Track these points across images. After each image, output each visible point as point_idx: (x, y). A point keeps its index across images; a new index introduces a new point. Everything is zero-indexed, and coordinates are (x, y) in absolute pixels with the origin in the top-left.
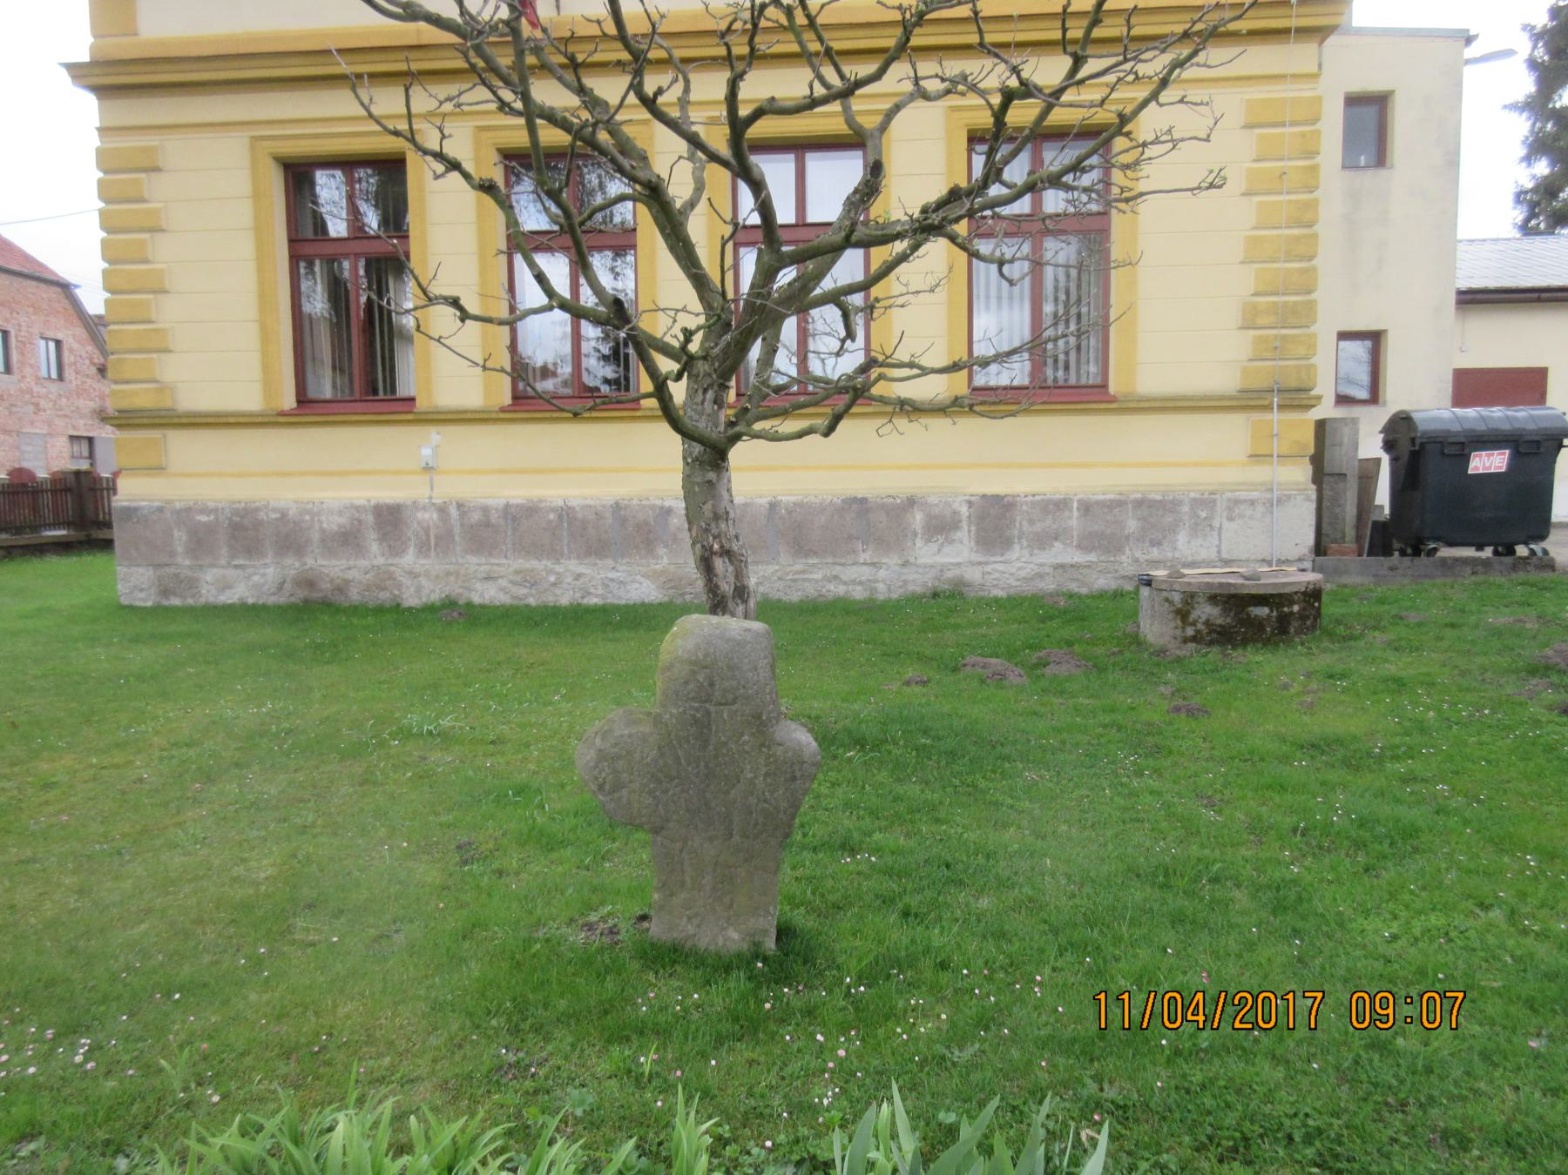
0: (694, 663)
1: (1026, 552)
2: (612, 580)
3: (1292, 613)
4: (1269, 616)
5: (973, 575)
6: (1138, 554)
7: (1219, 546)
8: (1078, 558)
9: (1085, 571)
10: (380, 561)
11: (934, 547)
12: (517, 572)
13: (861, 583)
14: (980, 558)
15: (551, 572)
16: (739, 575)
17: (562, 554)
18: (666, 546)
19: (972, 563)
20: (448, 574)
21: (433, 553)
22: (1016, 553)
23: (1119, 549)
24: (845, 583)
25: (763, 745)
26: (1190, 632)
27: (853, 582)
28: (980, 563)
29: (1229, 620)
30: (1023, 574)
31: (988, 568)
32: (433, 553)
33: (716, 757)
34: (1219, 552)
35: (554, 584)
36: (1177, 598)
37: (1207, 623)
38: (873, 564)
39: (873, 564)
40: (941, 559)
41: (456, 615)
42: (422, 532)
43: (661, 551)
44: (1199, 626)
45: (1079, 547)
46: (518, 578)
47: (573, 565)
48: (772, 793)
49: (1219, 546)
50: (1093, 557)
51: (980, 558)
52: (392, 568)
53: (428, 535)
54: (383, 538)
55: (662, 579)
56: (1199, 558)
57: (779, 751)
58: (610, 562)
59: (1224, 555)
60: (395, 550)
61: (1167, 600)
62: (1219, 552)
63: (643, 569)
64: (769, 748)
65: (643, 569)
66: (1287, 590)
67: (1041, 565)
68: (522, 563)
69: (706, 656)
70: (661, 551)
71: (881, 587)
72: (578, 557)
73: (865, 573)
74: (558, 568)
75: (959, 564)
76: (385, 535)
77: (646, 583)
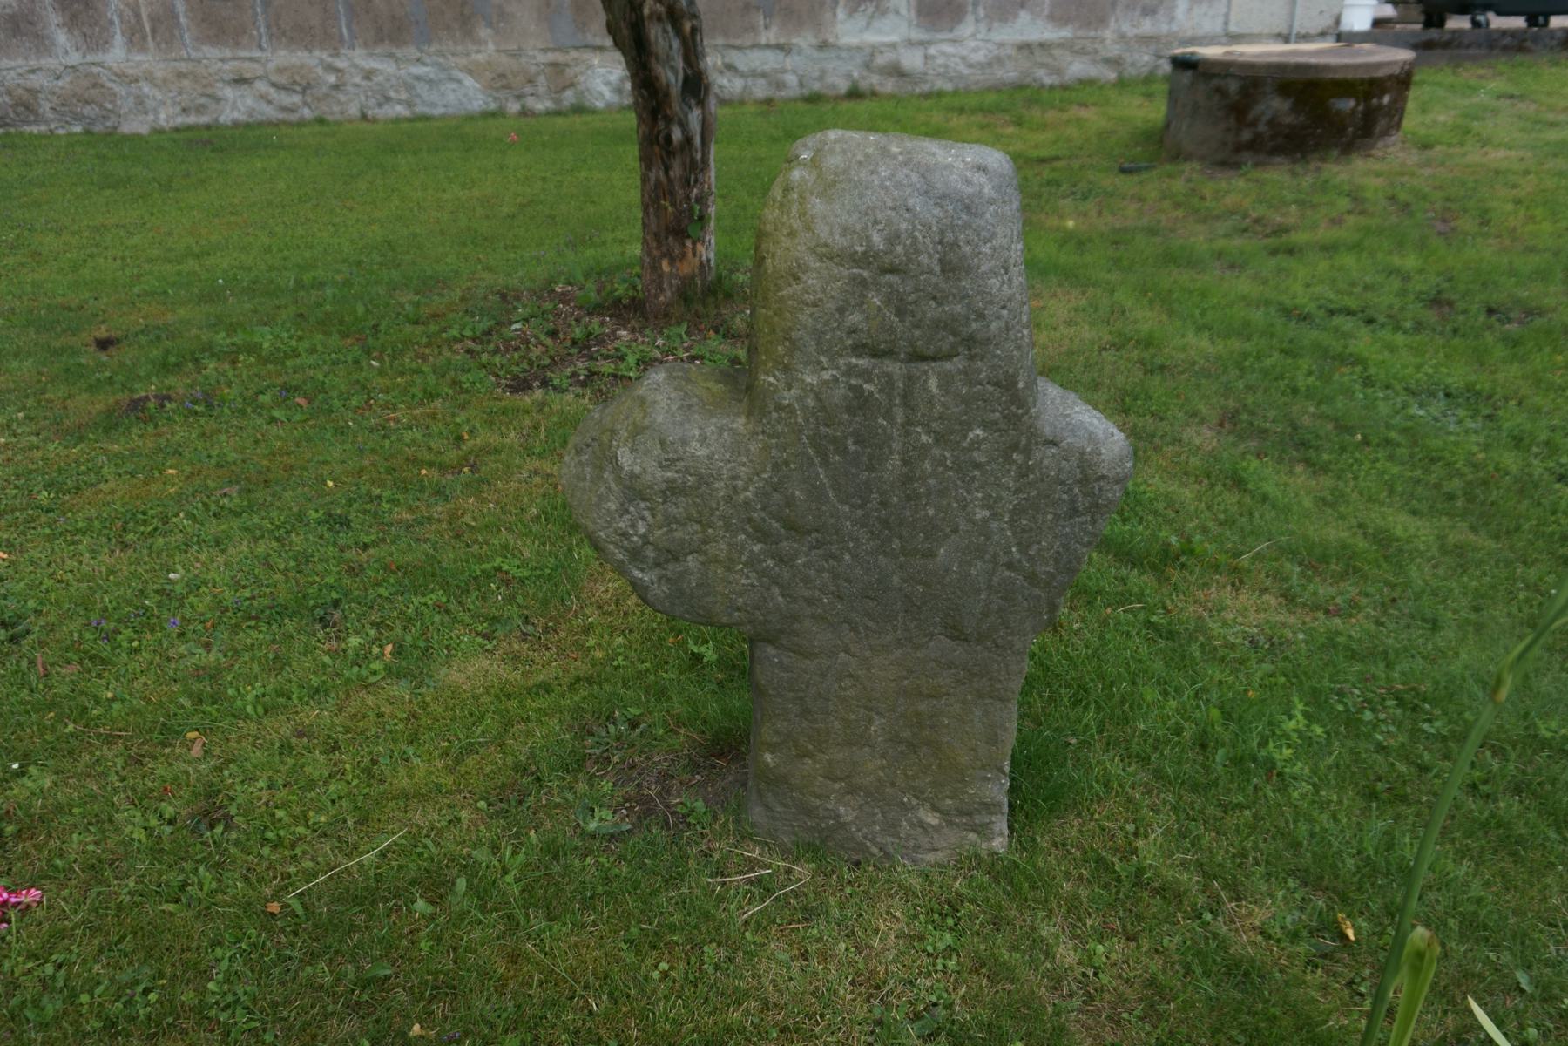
0: (865, 259)
1: (983, 27)
2: (418, 78)
3: (1380, 107)
4: (1353, 111)
5: (912, 60)
6: (1126, 27)
7: (1227, 16)
8: (1050, 33)
9: (1056, 52)
10: (75, 58)
11: (860, 20)
12: (280, 70)
13: (764, 75)
14: (924, 36)
15: (330, 68)
16: (692, 53)
17: (341, 40)
18: (490, 25)
19: (910, 43)
20: (180, 75)
21: (151, 43)
22: (967, 28)
23: (1102, 21)
24: (742, 75)
25: (1015, 447)
26: (1246, 135)
27: (754, 74)
28: (922, 43)
29: (1302, 118)
30: (979, 57)
31: (932, 51)
32: (151, 43)
33: (907, 480)
34: (1226, 23)
35: (336, 87)
36: (1233, 86)
37: (1272, 123)
38: (779, 47)
39: (779, 47)
40: (871, 38)
41: (208, 143)
42: (128, 13)
43: (484, 32)
44: (1262, 128)
45: (1051, 17)
46: (283, 80)
47: (357, 58)
48: (1023, 548)
49: (1227, 16)
50: (1066, 33)
51: (917, 35)
52: (95, 70)
53: (138, 16)
54: (72, 22)
55: (488, 75)
56: (1200, 32)
57: (1046, 457)
58: (412, 52)
59: (1233, 28)
60: (95, 39)
61: (1218, 90)
62: (1226, 23)
63: (463, 61)
64: (1027, 452)
65: (463, 61)
66: (1381, 73)
67: (1001, 45)
68: (283, 57)
69: (893, 239)
70: (484, 32)
71: (791, 79)
72: (366, 45)
73: (768, 60)
74: (340, 63)
75: (893, 46)
76: (74, 17)
77: (469, 81)
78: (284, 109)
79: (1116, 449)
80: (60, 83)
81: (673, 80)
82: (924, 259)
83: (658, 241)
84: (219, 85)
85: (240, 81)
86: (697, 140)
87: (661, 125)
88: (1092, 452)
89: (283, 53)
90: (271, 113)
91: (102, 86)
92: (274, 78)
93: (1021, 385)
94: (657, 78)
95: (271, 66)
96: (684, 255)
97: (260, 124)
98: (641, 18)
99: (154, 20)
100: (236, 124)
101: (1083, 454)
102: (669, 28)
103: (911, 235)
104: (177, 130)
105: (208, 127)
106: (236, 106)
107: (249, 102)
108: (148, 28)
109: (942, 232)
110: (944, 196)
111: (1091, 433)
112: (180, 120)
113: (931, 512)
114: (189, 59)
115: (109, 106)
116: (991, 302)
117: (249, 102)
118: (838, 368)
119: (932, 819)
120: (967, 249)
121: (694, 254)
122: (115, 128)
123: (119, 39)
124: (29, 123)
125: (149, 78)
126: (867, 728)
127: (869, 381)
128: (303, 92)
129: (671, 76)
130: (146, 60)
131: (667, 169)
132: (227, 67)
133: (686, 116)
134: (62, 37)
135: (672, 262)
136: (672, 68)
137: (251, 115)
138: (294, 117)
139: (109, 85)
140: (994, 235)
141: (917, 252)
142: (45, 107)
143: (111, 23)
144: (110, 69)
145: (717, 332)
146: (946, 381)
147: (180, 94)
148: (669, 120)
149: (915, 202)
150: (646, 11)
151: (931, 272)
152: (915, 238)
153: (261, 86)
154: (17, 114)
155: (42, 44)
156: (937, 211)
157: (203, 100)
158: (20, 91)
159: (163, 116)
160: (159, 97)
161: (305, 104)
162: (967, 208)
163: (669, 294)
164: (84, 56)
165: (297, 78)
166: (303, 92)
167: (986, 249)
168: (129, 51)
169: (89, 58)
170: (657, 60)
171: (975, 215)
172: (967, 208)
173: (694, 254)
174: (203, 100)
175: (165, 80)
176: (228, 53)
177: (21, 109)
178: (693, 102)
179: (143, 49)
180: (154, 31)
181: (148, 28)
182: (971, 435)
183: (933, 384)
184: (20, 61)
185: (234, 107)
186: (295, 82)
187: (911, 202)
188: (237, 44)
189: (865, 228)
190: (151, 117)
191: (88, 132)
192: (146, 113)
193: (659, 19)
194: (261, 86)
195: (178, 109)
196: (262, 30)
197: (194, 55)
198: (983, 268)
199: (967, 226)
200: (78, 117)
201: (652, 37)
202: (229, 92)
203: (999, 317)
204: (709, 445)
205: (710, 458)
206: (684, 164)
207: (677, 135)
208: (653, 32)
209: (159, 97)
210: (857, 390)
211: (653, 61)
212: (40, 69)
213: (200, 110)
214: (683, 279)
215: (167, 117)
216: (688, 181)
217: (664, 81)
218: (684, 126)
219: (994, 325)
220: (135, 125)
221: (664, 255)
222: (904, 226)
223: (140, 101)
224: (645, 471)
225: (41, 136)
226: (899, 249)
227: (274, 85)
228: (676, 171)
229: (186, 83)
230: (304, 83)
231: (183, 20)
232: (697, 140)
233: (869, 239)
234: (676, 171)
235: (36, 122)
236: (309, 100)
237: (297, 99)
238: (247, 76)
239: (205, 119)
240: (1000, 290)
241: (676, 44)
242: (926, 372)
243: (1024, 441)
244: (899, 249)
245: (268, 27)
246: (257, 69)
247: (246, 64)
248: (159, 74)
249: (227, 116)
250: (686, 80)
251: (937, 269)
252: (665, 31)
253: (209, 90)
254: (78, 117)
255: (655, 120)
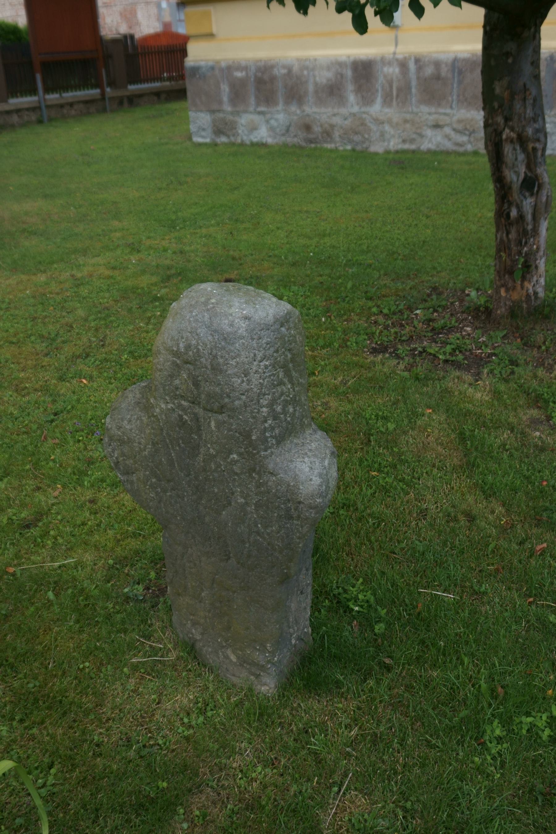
10: (356, 109)
12: (459, 121)
20: (406, 121)
21: (394, 103)
32: (394, 103)
46: (460, 127)
52: (364, 116)
53: (391, 87)
54: (359, 90)
60: (367, 101)
69: (188, 347)
78: (457, 144)
79: (311, 489)
80: (346, 122)
81: (515, 178)
82: (203, 360)
83: (500, 277)
84: (425, 128)
85: (437, 126)
86: (529, 217)
87: (506, 206)
88: (294, 486)
89: (463, 111)
90: (449, 146)
91: (366, 125)
92: (455, 126)
93: (254, 438)
94: (504, 178)
95: (455, 119)
96: (514, 288)
97: (442, 152)
98: (501, 140)
99: (399, 90)
100: (429, 151)
101: (289, 485)
102: (518, 148)
103: (196, 347)
104: (397, 152)
105: (413, 152)
106: (432, 140)
107: (439, 138)
108: (395, 93)
109: (211, 349)
110: (215, 331)
111: (296, 475)
112: (401, 146)
113: (216, 490)
114: (412, 112)
115: (366, 136)
116: (233, 390)
117: (439, 138)
118: (174, 404)
119: (233, 658)
120: (221, 361)
121: (522, 288)
122: (367, 148)
123: (379, 100)
124: (326, 142)
125: (390, 122)
126: (200, 594)
127: (186, 414)
128: (470, 135)
129: (515, 176)
130: (392, 113)
131: (508, 233)
132: (431, 118)
133: (522, 201)
134: (352, 98)
135: (507, 290)
136: (515, 172)
137: (438, 146)
138: (461, 150)
139: (369, 124)
140: (239, 355)
141: (199, 356)
142: (336, 134)
143: (377, 91)
144: (371, 116)
145: (522, 340)
146: (219, 424)
147: (403, 131)
148: (510, 204)
149: (202, 331)
150: (504, 137)
151: (206, 368)
152: (198, 349)
153: (447, 130)
154: (323, 137)
155: (342, 101)
156: (210, 338)
157: (414, 136)
158: (326, 125)
159: (392, 143)
160: (392, 132)
161: (470, 142)
162: (225, 339)
163: (503, 310)
164: (360, 108)
165: (468, 127)
166: (470, 135)
167: (233, 362)
168: (383, 106)
169: (363, 109)
170: (506, 167)
171: (229, 343)
172: (225, 339)
173: (522, 288)
174: (414, 136)
175: (397, 124)
176: (433, 110)
177: (325, 135)
178: (527, 194)
179: (390, 105)
180: (398, 96)
181: (395, 93)
182: (231, 456)
183: (213, 424)
184: (330, 109)
185: (430, 141)
186: (466, 129)
187: (199, 331)
188: (439, 105)
189: (178, 340)
190: (386, 144)
191: (353, 150)
192: (384, 141)
193: (512, 141)
194: (447, 130)
195: (400, 140)
196: (455, 97)
197: (415, 110)
198: (229, 372)
199: (223, 348)
200: (350, 141)
201: (505, 153)
202: (429, 132)
203: (240, 399)
204: (132, 424)
205: (131, 430)
206: (518, 231)
207: (514, 213)
208: (506, 150)
209: (392, 132)
210: (181, 416)
211: (504, 166)
212: (338, 114)
213: (412, 141)
214: (513, 302)
215: (394, 144)
216: (520, 242)
217: (508, 179)
218: (519, 208)
219: (237, 403)
220: (378, 148)
221: (503, 286)
222: (194, 342)
223: (382, 134)
224: (111, 428)
225: (331, 151)
226: (191, 353)
227: (454, 130)
228: (513, 235)
229: (408, 126)
230: (471, 130)
231: (414, 90)
232: (529, 217)
233: (178, 345)
234: (513, 235)
235: (330, 142)
236: (472, 139)
237: (465, 139)
238: (441, 123)
239: (413, 147)
240: (240, 385)
241: (521, 157)
242: (210, 418)
243: (258, 469)
244: (191, 353)
245: (458, 96)
246: (447, 120)
247: (442, 117)
248: (395, 120)
249: (426, 145)
250: (525, 180)
251: (209, 367)
252: (514, 149)
253: (419, 131)
254: (350, 141)
255: (503, 203)
